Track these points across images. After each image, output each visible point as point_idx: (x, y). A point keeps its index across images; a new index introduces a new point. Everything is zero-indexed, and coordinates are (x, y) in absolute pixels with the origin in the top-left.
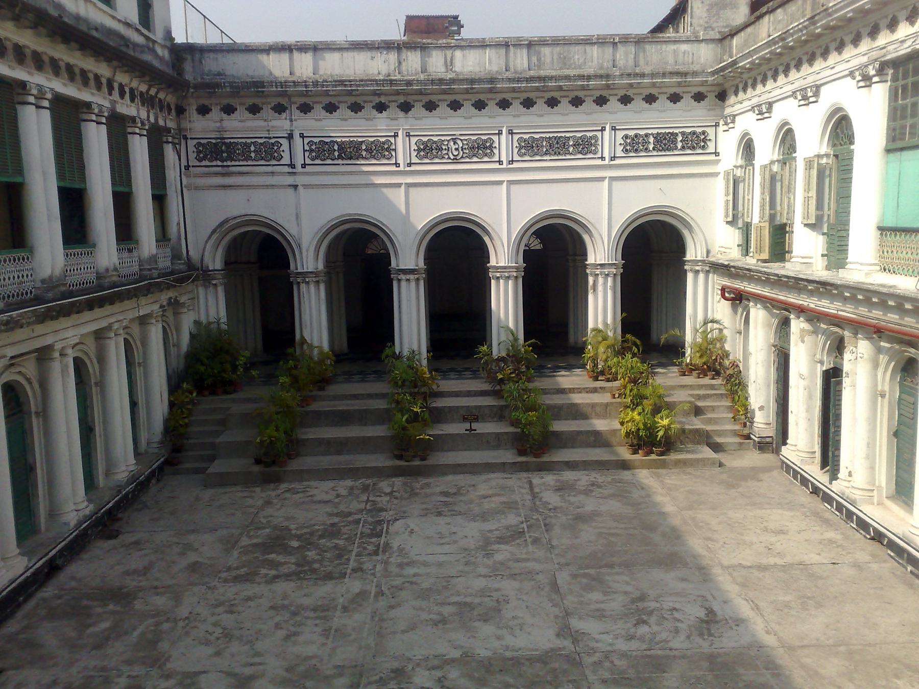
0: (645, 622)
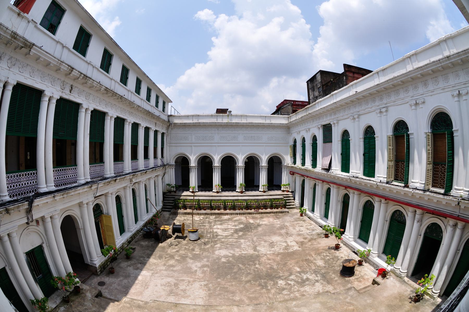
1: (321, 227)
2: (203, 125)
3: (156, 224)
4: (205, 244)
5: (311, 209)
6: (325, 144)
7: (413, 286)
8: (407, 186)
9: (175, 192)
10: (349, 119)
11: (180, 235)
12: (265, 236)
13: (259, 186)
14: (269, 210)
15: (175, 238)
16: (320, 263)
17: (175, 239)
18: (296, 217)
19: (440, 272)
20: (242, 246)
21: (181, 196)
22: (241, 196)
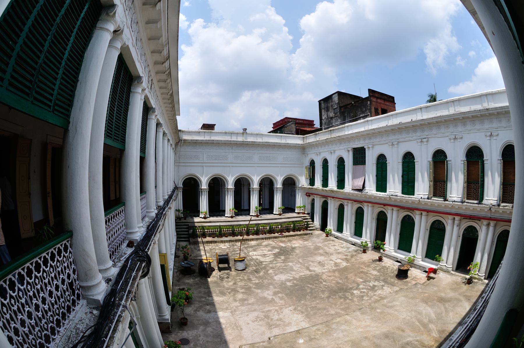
2: (216, 143)
6: (354, 166)
7: (460, 277)
8: (446, 200)
14: (292, 233)
16: (375, 273)
19: (481, 259)
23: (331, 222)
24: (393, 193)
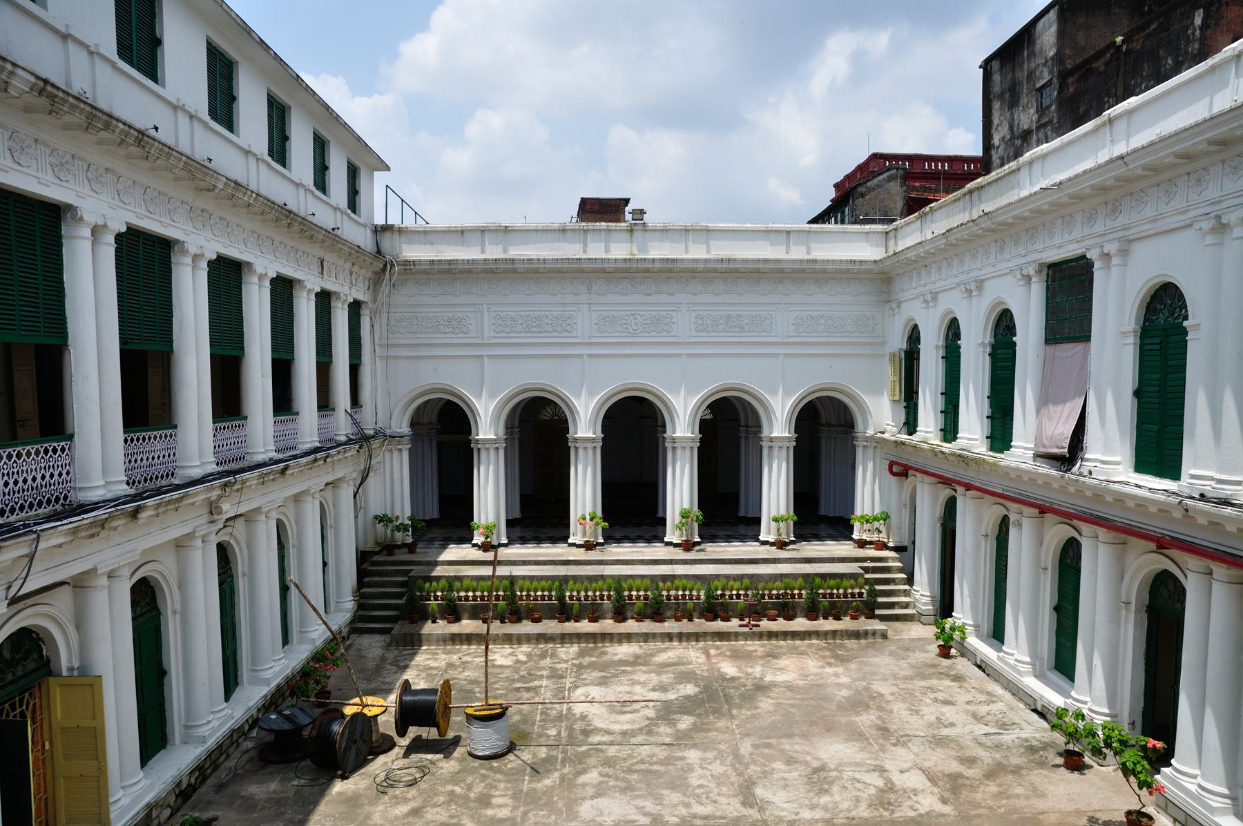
0: (826, 791)
1: (1042, 715)
2: (528, 271)
3: (324, 693)
4: (536, 770)
5: (987, 625)
6: (1051, 348)
9: (411, 548)
10: (1010, 277)
11: (430, 733)
12: (790, 736)
13: (757, 521)
14: (800, 624)
15: (408, 752)
17: (407, 754)
18: (919, 657)
20: (694, 781)
21: (436, 564)
22: (685, 562)
23: (966, 593)
24: (1209, 488)
